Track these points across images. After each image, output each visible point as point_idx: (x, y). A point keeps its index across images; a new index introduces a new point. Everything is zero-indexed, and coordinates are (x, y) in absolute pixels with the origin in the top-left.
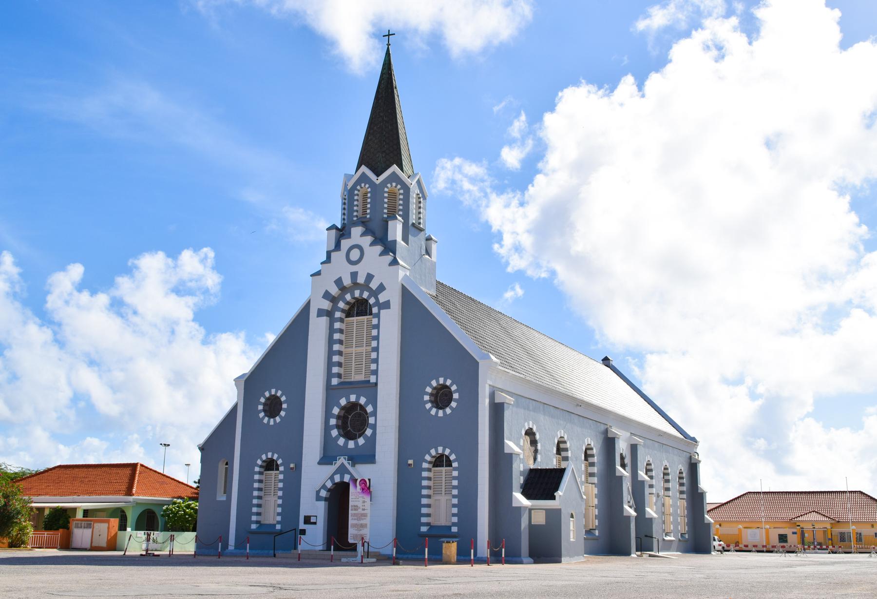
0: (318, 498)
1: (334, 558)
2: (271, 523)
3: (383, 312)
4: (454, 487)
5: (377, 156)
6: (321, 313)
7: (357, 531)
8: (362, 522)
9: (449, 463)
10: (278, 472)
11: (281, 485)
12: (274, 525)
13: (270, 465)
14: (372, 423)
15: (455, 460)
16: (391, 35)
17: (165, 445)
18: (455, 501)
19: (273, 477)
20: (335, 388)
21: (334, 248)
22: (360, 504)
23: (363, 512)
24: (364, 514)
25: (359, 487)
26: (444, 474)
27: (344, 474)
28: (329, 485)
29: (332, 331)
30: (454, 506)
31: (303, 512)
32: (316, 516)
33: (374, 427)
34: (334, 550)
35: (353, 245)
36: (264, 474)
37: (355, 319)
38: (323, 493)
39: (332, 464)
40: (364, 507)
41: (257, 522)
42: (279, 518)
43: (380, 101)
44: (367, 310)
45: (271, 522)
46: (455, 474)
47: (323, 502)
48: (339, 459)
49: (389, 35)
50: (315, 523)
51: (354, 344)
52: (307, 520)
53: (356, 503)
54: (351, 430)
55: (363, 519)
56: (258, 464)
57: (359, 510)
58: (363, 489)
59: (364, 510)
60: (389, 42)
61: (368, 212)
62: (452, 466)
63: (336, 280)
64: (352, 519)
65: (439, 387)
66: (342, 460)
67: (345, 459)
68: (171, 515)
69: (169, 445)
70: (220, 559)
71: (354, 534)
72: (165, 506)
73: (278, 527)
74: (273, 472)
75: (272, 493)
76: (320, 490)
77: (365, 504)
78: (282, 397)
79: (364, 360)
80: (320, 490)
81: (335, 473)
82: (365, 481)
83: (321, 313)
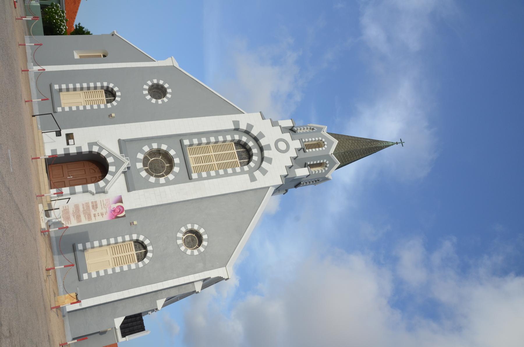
3: (247, 176)
6: (236, 123)
8: (82, 216)
10: (105, 103)
12: (60, 106)
13: (110, 94)
19: (101, 98)
20: (181, 142)
22: (99, 210)
24: (91, 217)
25: (115, 206)
26: (130, 253)
28: (104, 153)
31: (75, 131)
32: (74, 144)
33: (157, 185)
36: (102, 90)
37: (235, 151)
38: (95, 149)
39: (121, 154)
40: (97, 215)
43: (370, 144)
44: (242, 160)
45: (63, 102)
47: (119, 242)
50: (68, 144)
53: (99, 206)
54: (150, 161)
55: (85, 216)
57: (93, 211)
58: (114, 211)
59: (95, 216)
60: (399, 143)
61: (310, 150)
62: (138, 262)
63: (262, 134)
71: (68, 209)
73: (59, 109)
75: (87, 99)
76: (98, 145)
77: (101, 216)
78: (167, 99)
80: (98, 145)
81: (115, 157)
82: (122, 212)
83: (236, 123)
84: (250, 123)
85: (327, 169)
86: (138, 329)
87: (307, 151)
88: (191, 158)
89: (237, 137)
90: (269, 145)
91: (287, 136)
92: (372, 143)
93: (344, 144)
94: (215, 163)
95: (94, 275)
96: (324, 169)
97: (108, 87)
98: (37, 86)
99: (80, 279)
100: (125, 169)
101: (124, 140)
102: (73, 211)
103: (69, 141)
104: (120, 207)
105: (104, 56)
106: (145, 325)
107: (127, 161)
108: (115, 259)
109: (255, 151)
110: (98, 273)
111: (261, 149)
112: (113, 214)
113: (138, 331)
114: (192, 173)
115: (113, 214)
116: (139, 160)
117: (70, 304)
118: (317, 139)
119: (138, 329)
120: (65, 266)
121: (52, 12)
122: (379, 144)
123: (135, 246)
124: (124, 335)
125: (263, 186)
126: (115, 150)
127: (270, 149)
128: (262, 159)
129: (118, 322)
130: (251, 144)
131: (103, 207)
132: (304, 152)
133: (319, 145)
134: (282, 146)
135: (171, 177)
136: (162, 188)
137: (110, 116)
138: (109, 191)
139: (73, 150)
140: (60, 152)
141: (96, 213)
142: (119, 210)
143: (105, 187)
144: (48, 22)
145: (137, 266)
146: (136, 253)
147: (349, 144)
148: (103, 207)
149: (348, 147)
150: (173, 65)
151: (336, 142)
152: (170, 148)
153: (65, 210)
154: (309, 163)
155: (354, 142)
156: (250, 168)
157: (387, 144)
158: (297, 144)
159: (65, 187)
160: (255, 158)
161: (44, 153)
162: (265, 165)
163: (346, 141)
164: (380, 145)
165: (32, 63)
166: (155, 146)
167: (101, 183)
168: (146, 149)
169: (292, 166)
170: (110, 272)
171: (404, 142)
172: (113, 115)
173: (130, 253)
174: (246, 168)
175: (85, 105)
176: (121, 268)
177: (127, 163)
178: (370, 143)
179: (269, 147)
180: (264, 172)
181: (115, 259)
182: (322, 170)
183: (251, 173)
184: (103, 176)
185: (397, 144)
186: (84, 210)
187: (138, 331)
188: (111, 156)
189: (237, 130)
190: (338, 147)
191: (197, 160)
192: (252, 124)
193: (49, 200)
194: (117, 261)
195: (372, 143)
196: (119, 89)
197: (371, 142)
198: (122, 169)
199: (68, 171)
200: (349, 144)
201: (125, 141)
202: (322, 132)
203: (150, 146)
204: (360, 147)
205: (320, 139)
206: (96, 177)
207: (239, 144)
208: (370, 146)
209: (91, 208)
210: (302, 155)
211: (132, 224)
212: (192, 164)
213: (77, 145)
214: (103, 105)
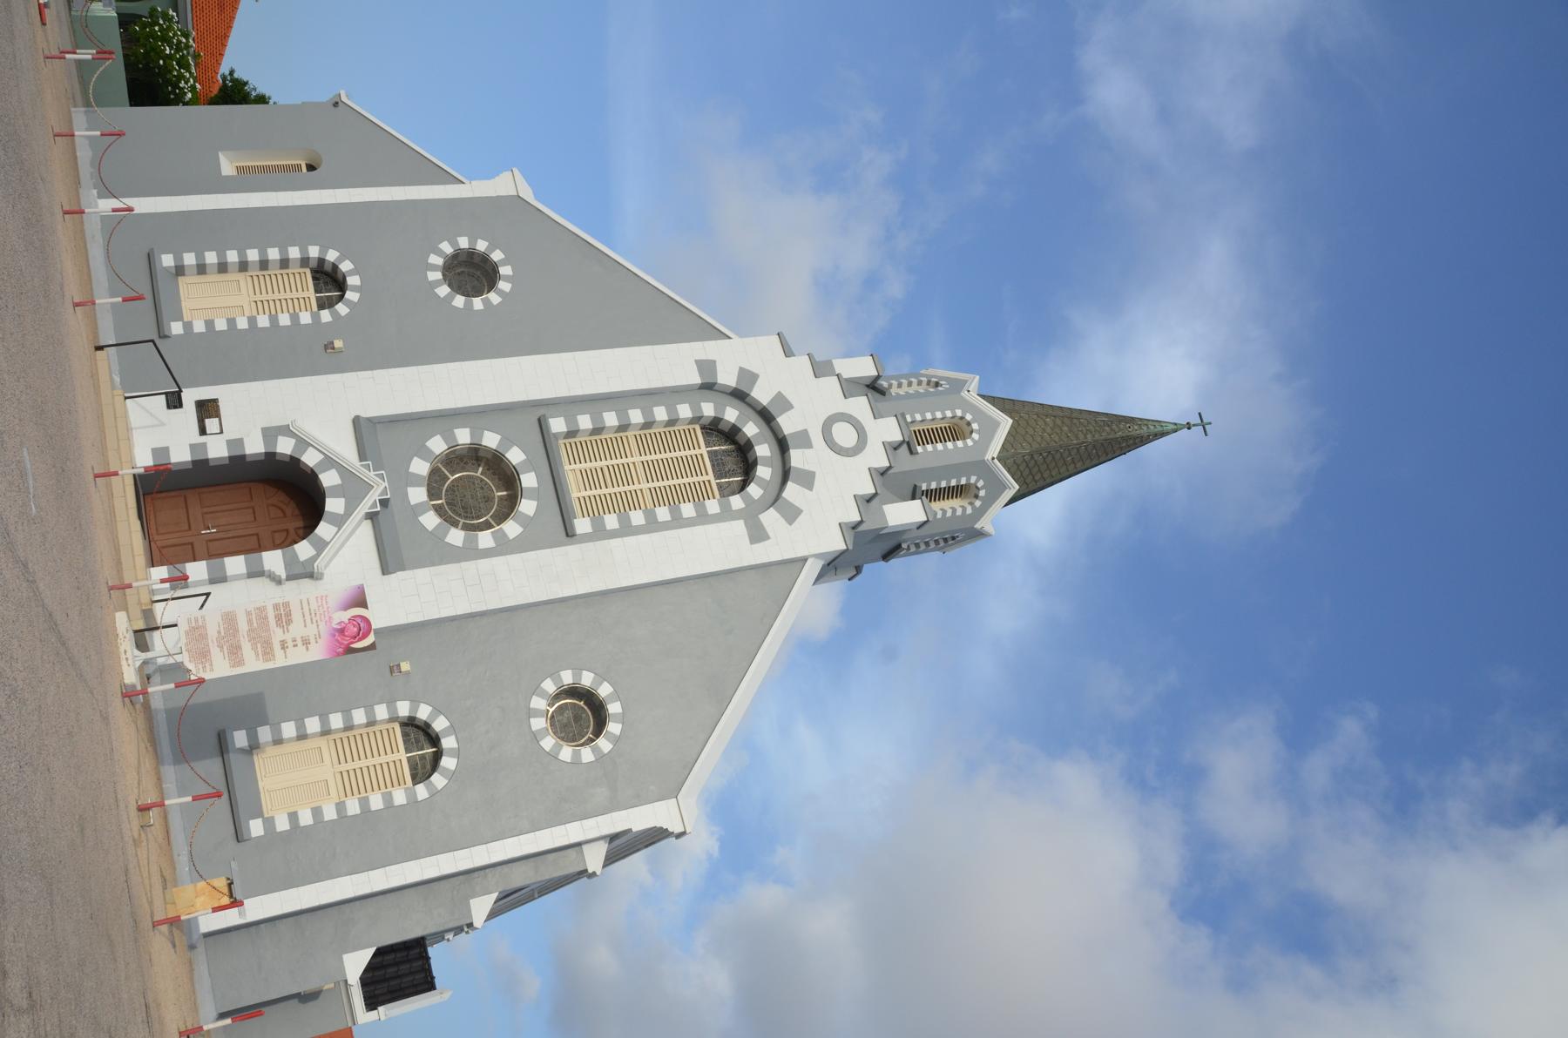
2: (183, 304)
3: (739, 527)
6: (706, 366)
7: (216, 635)
10: (315, 307)
12: (179, 318)
13: (329, 280)
14: (317, 252)
16: (1204, 428)
19: (301, 294)
20: (542, 424)
21: (845, 376)
22: (297, 629)
24: (272, 649)
26: (390, 758)
27: (344, 497)
28: (310, 459)
32: (222, 432)
33: (470, 553)
35: (864, 432)
38: (285, 447)
40: (290, 644)
43: (1107, 428)
44: (726, 477)
45: (187, 305)
46: (305, 318)
50: (203, 431)
53: (296, 616)
55: (254, 648)
57: (279, 631)
58: (342, 631)
59: (283, 645)
60: (1194, 425)
62: (414, 784)
65: (340, 277)
67: (385, 491)
68: (157, 28)
71: (204, 627)
72: (175, 14)
73: (176, 328)
74: (311, 293)
75: (258, 297)
76: (293, 435)
77: (301, 648)
80: (293, 435)
81: (344, 471)
82: (365, 636)
83: (706, 366)
85: (978, 503)
86: (416, 986)
87: (920, 449)
88: (571, 472)
89: (708, 410)
91: (860, 406)
93: (1030, 431)
95: (282, 824)
96: (971, 504)
98: (108, 253)
99: (239, 835)
100: (374, 505)
101: (369, 420)
102: (219, 632)
103: (207, 421)
104: (359, 620)
105: (311, 168)
106: (435, 973)
108: (345, 774)
109: (763, 450)
110: (293, 816)
111: (782, 445)
112: (337, 640)
115: (337, 640)
116: (414, 480)
117: (211, 911)
121: (153, 35)
122: (1136, 427)
123: (405, 735)
128: (785, 474)
129: (356, 963)
130: (751, 429)
131: (308, 621)
133: (954, 431)
134: (845, 435)
135: (511, 528)
137: (329, 346)
138: (327, 573)
139: (217, 450)
140: (180, 455)
141: (288, 637)
142: (356, 629)
147: (1044, 430)
148: (308, 621)
152: (508, 441)
155: (1059, 422)
156: (749, 501)
157: (1159, 429)
158: (888, 430)
160: (763, 472)
162: (792, 491)
164: (1138, 432)
166: (463, 437)
167: (303, 549)
168: (438, 445)
169: (876, 494)
170: (330, 814)
171: (1210, 423)
172: (338, 344)
173: (390, 758)
174: (736, 502)
175: (255, 313)
176: (364, 802)
177: (382, 488)
178: (1108, 426)
179: (804, 440)
181: (345, 774)
183: (751, 517)
185: (1189, 428)
189: (709, 387)
191: (590, 478)
194: (352, 785)
198: (365, 506)
199: (204, 514)
202: (964, 394)
204: (1077, 438)
205: (959, 413)
207: (715, 430)
208: (1109, 434)
210: (905, 462)
211: (394, 669)
212: (575, 491)
213: (229, 433)
214: (308, 313)
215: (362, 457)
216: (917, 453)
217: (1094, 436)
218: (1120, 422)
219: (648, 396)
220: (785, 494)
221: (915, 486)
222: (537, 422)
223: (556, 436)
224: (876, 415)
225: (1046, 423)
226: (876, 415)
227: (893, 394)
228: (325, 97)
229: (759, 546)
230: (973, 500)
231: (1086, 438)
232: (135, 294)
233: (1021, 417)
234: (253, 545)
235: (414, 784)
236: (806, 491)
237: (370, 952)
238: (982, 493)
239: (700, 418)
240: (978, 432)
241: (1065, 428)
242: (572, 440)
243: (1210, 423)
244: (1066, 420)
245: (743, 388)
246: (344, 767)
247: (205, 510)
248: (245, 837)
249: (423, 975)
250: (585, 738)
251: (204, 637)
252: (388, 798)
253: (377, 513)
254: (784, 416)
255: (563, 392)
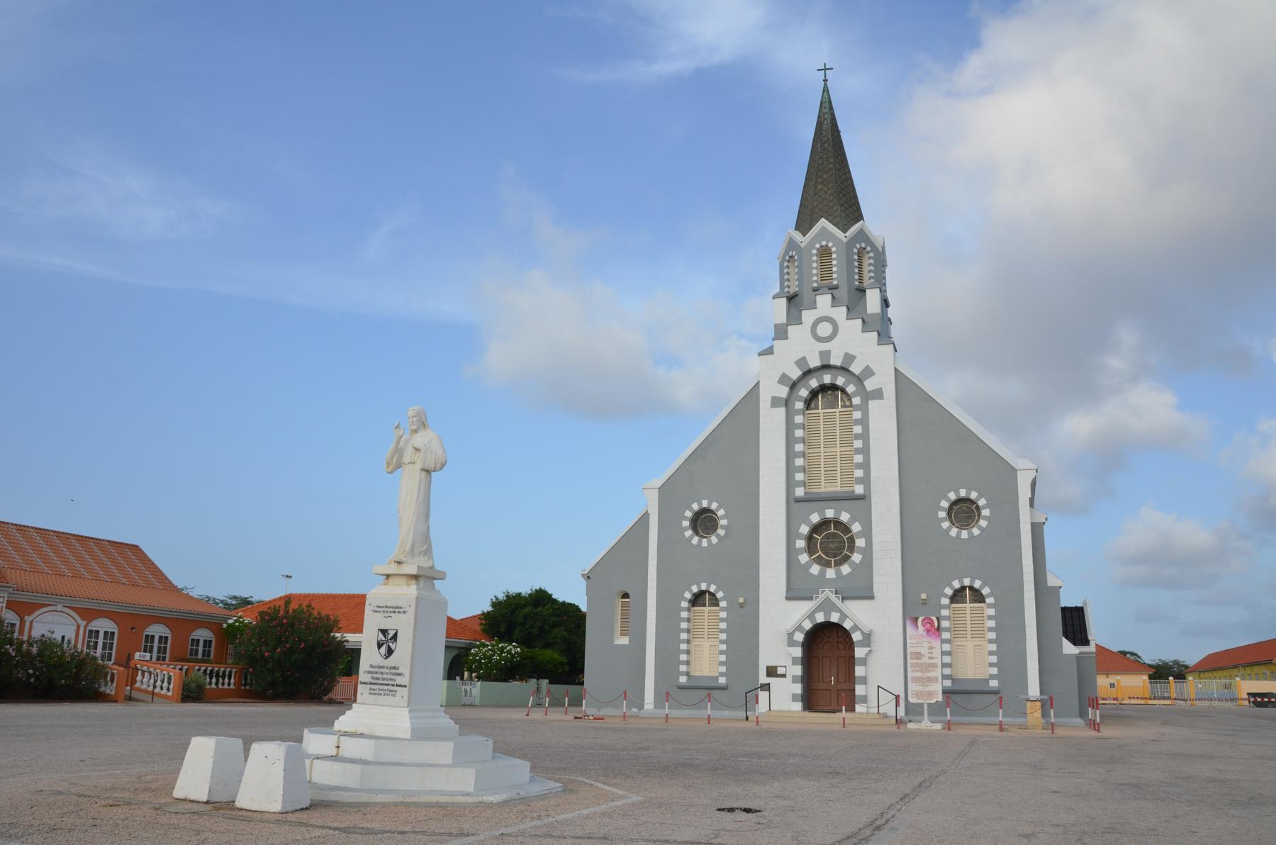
0: (791, 643)
1: (711, 717)
3: (873, 404)
4: (722, 631)
5: (835, 209)
6: (775, 402)
8: (929, 675)
9: (715, 601)
11: (723, 625)
15: (723, 599)
17: (287, 576)
18: (723, 647)
20: (798, 500)
22: (924, 651)
23: (931, 661)
26: (968, 612)
28: (808, 625)
29: (790, 426)
30: (721, 652)
31: (764, 662)
33: (868, 552)
34: (668, 708)
38: (800, 637)
39: (812, 599)
40: (931, 655)
41: (687, 674)
42: (723, 669)
43: (826, 145)
45: (706, 673)
46: (723, 615)
48: (823, 592)
49: (825, 69)
50: (784, 676)
51: (822, 444)
52: (772, 672)
53: (918, 650)
56: (685, 598)
57: (924, 659)
58: (928, 631)
64: (913, 671)
66: (828, 593)
67: (832, 592)
69: (290, 577)
70: (951, 732)
76: (793, 632)
79: (839, 465)
80: (794, 632)
82: (932, 621)
83: (775, 402)
84: (777, 379)
85: (869, 249)
86: (1079, 618)
87: (835, 282)
88: (825, 488)
89: (800, 405)
90: (821, 353)
91: (808, 316)
92: (824, 139)
93: (825, 202)
94: (838, 449)
95: (994, 671)
96: (868, 253)
97: (690, 601)
99: (995, 692)
100: (838, 598)
101: (787, 591)
103: (778, 673)
104: (924, 622)
105: (626, 596)
106: (1074, 605)
107: (825, 593)
108: (973, 636)
109: (827, 379)
110: (991, 665)
111: (826, 367)
113: (1081, 619)
114: (854, 491)
116: (822, 573)
118: (815, 258)
119: (1079, 618)
120: (1001, 708)
121: (486, 664)
122: (825, 123)
123: (957, 602)
124: (1086, 642)
125: (893, 380)
126: (804, 607)
127: (829, 352)
128: (844, 369)
129: (1069, 648)
130: (814, 383)
132: (837, 288)
133: (825, 253)
134: (825, 329)
135: (856, 528)
136: (875, 547)
137: (742, 606)
138: (869, 628)
139: (798, 670)
140: (798, 689)
141: (927, 655)
142: (928, 625)
143: (862, 633)
144: (251, 668)
145: (990, 606)
146: (970, 603)
147: (826, 192)
149: (830, 195)
150: (657, 490)
151: (823, 223)
152: (807, 521)
153: (917, 695)
154: (857, 283)
155: (820, 180)
156: (856, 394)
157: (827, 105)
158: (824, 300)
159: (854, 690)
160: (840, 381)
161: (797, 712)
162: (856, 368)
163: (819, 196)
164: (829, 122)
165: (631, 709)
166: (801, 544)
167: (856, 637)
168: (804, 558)
169: (862, 319)
170: (993, 647)
171: (825, 64)
172: (741, 600)
173: (968, 612)
174: (856, 401)
175: (718, 640)
176: (990, 629)
177: (829, 592)
178: (824, 143)
179: (825, 354)
180: (868, 372)
181: (973, 636)
182: (870, 265)
183: (868, 396)
184: (846, 634)
185: (827, 80)
186: (922, 671)
187: (1081, 619)
188: (814, 615)
189: (787, 403)
190: (830, 217)
191: (830, 478)
192: (781, 374)
193: (877, 716)
194: (978, 633)
195: (824, 139)
196: (696, 584)
197: (822, 140)
198: (838, 602)
199: (823, 681)
200: (826, 192)
201: (789, 589)
202: (803, 245)
203: (800, 551)
204: (831, 169)
205: (814, 252)
206: (838, 642)
207: (810, 402)
208: (829, 145)
209: (919, 661)
210: (843, 293)
211: (924, 603)
212: (836, 488)
213: (789, 663)
214: (721, 613)
215: (811, 599)
216: (837, 285)
217: (831, 157)
218: (821, 134)
219: (790, 440)
220: (857, 373)
221: (856, 289)
222: (1054, 704)
223: (806, 493)
224: (813, 306)
225: (821, 189)
226: (813, 306)
227: (797, 289)
228: (583, 584)
229: (885, 395)
230: (866, 251)
231: (832, 163)
232: (623, 695)
233: (816, 207)
234: (850, 661)
235: (984, 602)
236: (856, 360)
237: (1064, 640)
238: (863, 245)
239: (803, 410)
240: (828, 242)
241: (825, 176)
242: (807, 484)
243: (825, 64)
244: (820, 173)
245: (791, 383)
246: (969, 636)
247: (821, 681)
248: (998, 689)
249: (1074, 612)
250: (975, 511)
251: (921, 692)
252: (990, 618)
253: (842, 597)
254: (809, 363)
255: (783, 486)
